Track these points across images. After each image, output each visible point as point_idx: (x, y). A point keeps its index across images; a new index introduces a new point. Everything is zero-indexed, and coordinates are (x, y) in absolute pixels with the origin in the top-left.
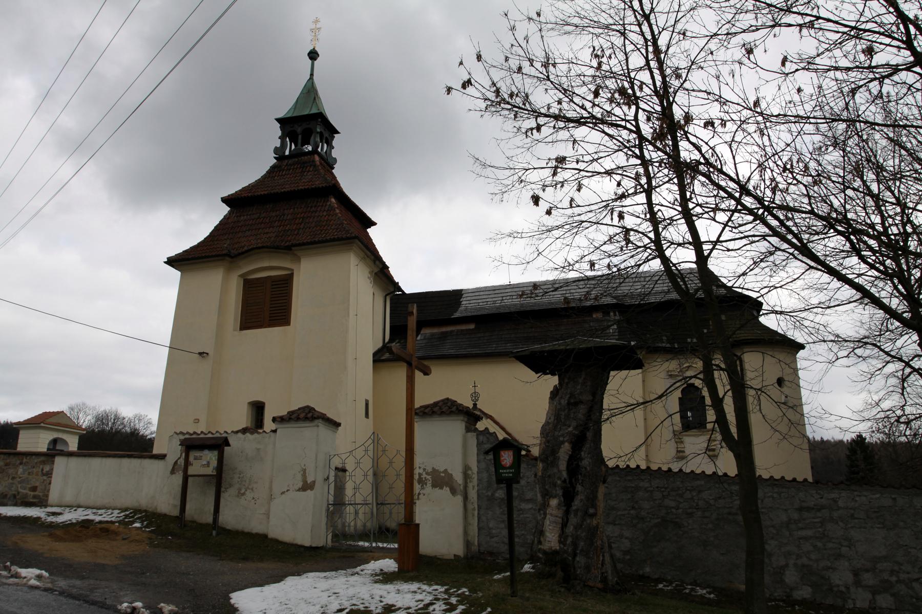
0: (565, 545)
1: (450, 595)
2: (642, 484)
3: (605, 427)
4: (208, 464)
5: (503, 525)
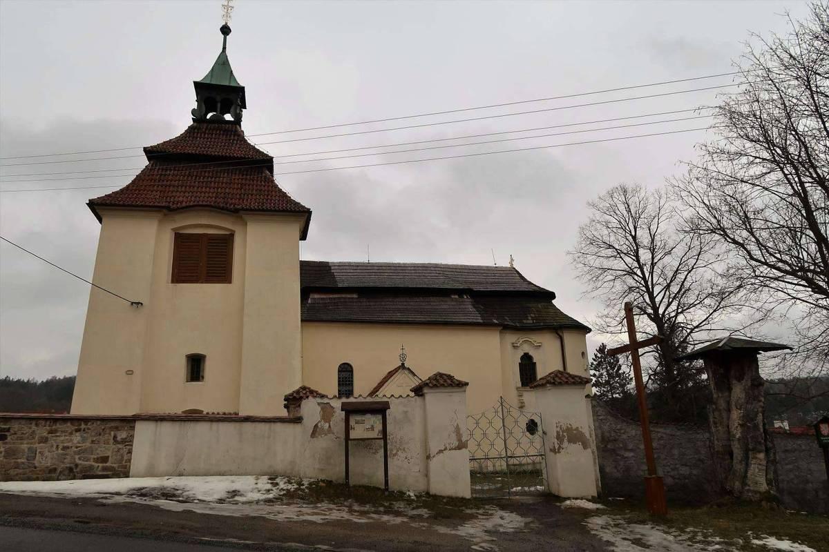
4: (372, 428)
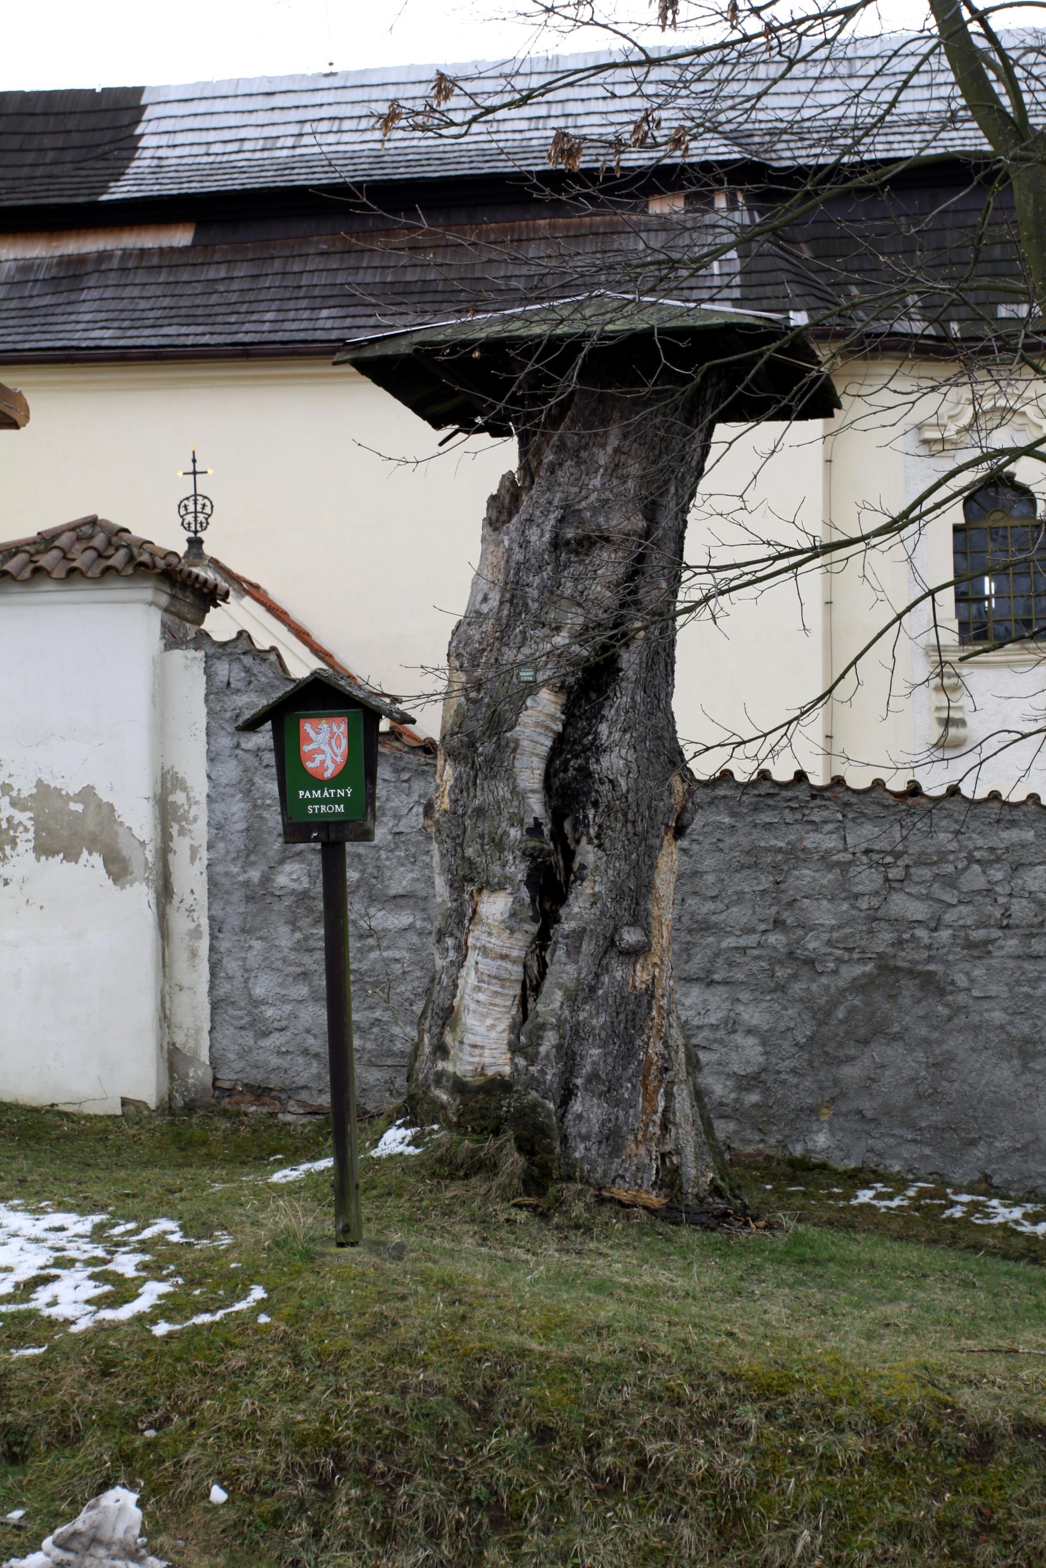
0: (532, 1060)
1: (115, 1246)
2: (811, 840)
3: (690, 638)
5: (302, 990)
